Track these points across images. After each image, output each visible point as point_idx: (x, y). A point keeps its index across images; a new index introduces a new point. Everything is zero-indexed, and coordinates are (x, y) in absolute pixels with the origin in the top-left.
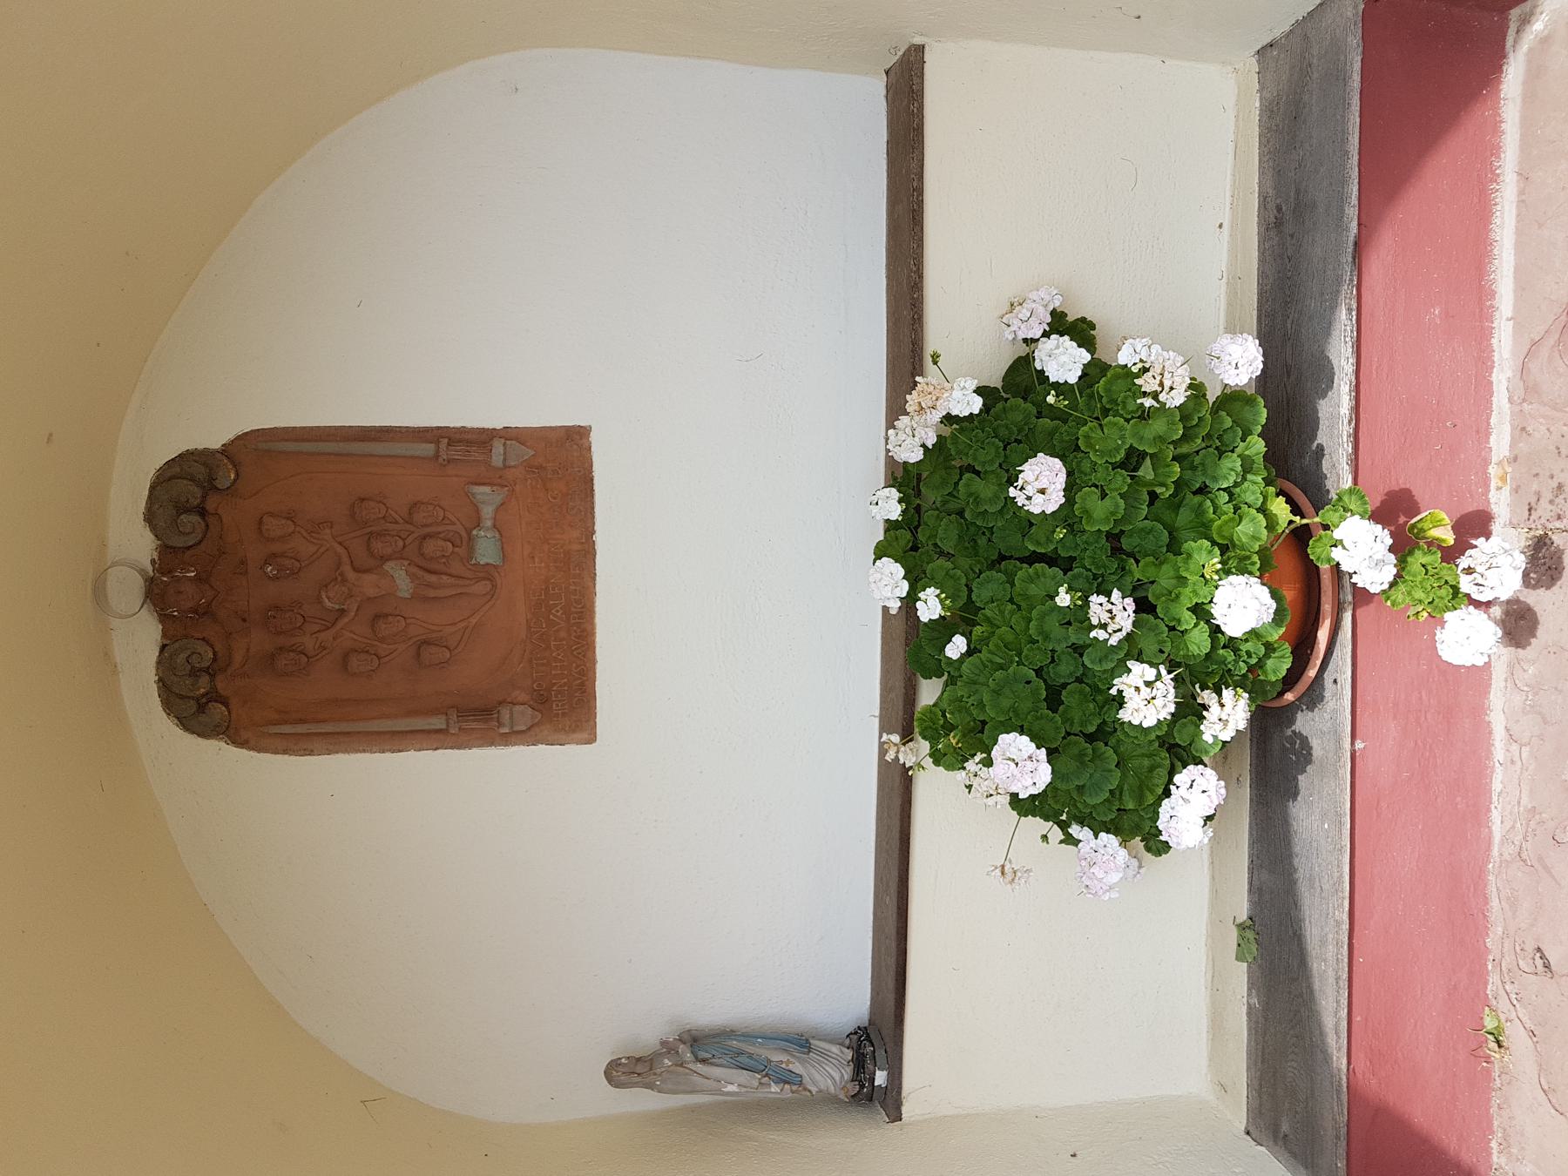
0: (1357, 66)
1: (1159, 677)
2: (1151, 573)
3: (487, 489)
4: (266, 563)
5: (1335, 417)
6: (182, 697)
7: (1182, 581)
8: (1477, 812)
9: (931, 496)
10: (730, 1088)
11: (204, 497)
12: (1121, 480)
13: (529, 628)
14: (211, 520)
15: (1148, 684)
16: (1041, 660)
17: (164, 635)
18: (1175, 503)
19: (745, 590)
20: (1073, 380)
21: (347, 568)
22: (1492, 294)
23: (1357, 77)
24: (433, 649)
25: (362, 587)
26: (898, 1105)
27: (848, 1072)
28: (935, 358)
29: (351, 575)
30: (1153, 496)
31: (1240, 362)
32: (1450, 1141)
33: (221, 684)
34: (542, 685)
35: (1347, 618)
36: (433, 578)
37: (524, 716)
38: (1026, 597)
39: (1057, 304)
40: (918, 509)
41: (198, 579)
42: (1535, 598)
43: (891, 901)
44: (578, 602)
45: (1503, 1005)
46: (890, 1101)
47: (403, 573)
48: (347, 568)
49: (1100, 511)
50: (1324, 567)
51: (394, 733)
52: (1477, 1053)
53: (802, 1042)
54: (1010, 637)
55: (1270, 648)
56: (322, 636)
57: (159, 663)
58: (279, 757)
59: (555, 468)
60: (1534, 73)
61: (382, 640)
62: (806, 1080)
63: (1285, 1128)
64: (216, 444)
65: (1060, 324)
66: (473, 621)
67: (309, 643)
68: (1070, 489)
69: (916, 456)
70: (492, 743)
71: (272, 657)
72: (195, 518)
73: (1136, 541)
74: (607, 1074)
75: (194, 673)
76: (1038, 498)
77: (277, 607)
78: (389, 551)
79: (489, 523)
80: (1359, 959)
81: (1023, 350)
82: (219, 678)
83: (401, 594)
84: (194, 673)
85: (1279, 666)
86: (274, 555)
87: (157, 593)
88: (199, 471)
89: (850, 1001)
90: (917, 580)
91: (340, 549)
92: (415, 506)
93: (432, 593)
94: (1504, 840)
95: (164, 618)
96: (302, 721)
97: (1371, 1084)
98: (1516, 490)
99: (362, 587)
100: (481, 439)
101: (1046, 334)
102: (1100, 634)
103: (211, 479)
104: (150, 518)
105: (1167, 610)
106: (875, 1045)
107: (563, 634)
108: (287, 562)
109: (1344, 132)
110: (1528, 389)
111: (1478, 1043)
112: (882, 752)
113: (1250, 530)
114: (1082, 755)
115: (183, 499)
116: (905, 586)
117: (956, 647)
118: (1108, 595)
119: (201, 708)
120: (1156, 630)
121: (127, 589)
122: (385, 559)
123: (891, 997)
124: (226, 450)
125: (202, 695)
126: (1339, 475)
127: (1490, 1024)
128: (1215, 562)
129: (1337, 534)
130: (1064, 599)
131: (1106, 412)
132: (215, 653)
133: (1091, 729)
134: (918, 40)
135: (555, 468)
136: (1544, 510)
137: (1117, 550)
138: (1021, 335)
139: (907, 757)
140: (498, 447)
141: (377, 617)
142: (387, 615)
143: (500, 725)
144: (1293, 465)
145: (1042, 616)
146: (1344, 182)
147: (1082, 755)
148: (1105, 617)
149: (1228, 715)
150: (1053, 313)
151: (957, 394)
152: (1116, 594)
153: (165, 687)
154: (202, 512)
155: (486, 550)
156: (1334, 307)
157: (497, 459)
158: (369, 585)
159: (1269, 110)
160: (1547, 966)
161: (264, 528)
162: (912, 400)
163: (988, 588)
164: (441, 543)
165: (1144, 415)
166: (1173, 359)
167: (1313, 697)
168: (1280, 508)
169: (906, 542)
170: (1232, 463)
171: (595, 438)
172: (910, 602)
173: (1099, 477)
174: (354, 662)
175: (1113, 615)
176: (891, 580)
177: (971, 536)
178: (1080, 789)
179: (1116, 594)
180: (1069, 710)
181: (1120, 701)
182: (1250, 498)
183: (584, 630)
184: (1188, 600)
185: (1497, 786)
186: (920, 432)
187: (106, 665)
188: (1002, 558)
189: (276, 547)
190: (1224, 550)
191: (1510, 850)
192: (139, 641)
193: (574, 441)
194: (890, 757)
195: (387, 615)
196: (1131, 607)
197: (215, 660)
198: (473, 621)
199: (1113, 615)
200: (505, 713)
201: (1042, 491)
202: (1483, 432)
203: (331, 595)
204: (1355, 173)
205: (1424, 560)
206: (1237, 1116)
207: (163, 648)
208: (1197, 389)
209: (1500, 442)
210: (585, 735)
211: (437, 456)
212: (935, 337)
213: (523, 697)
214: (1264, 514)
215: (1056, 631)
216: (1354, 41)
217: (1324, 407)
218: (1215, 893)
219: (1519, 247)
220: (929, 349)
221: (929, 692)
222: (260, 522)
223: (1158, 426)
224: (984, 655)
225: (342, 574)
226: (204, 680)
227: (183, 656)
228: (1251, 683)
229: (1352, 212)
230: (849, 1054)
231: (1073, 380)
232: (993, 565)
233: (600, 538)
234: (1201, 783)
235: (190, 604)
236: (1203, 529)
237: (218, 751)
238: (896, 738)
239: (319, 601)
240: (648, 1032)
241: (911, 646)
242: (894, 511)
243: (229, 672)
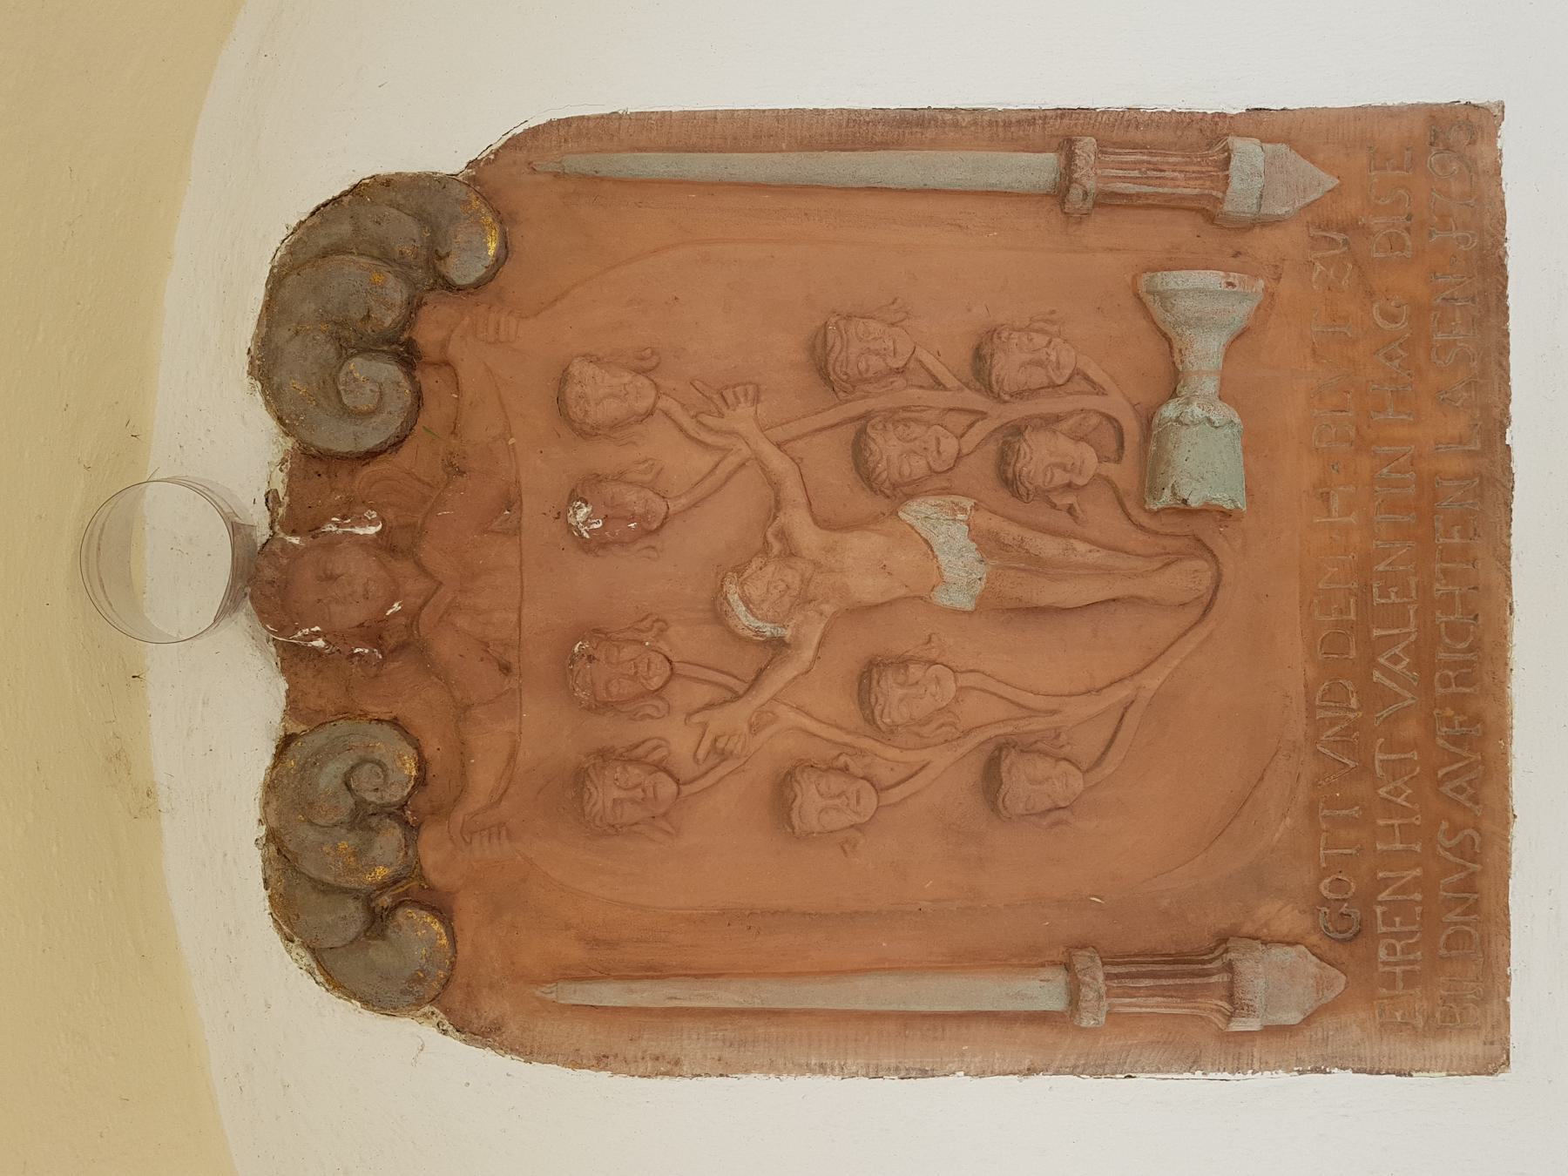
3: (1212, 279)
4: (575, 497)
6: (326, 889)
11: (414, 306)
13: (1311, 709)
14: (430, 380)
17: (294, 707)
21: (798, 521)
24: (1042, 767)
29: (808, 537)
33: (434, 853)
36: (1049, 547)
37: (1279, 979)
41: (386, 546)
44: (1455, 631)
47: (960, 533)
48: (798, 521)
51: (908, 1019)
56: (719, 720)
57: (271, 787)
58: (586, 1074)
61: (887, 735)
64: (450, 159)
66: (1152, 682)
67: (680, 741)
70: (1193, 1063)
71: (580, 778)
72: (388, 371)
75: (363, 818)
77: (598, 633)
78: (918, 466)
79: (1210, 386)
83: (942, 598)
84: (363, 818)
86: (598, 479)
88: (405, 234)
91: (778, 462)
95: (293, 658)
96: (654, 972)
103: (435, 257)
104: (266, 365)
107: (1411, 729)
108: (632, 498)
115: (356, 314)
119: (377, 922)
121: (186, 563)
122: (902, 491)
124: (482, 178)
125: (377, 893)
132: (422, 765)
142: (903, 662)
153: (281, 853)
154: (408, 356)
157: (1241, 195)
158: (862, 564)
161: (573, 391)
164: (1065, 445)
171: (1510, 139)
174: (810, 797)
183: (1477, 719)
187: (121, 777)
189: (603, 456)
192: (221, 711)
193: (1456, 141)
195: (903, 662)
197: (421, 781)
198: (1152, 682)
203: (755, 590)
207: (286, 743)
210: (1471, 1046)
211: (1060, 193)
222: (564, 378)
225: (783, 535)
226: (389, 840)
227: (329, 776)
235: (355, 614)
237: (415, 1047)
239: (718, 614)
243: (459, 816)
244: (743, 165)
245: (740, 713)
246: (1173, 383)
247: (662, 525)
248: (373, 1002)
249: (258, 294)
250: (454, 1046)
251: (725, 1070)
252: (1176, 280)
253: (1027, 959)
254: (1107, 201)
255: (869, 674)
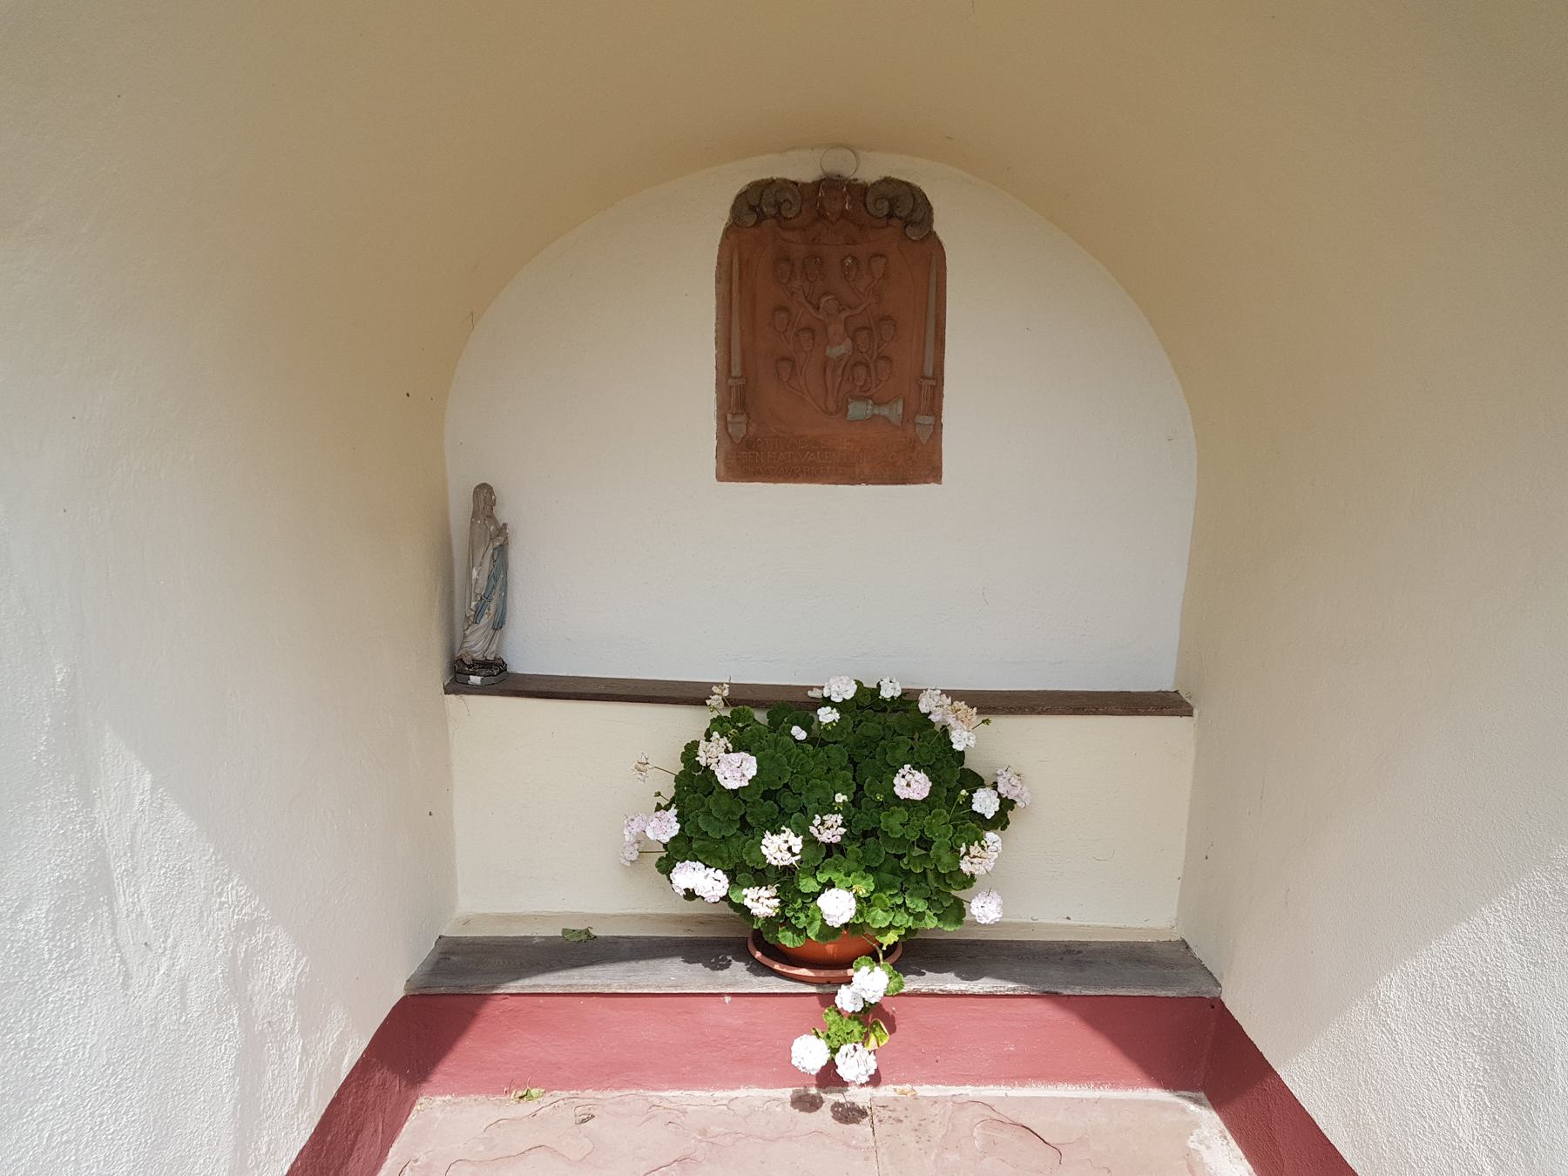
0: (1170, 994)
1: (794, 855)
2: (852, 856)
4: (854, 258)
5: (946, 982)
7: (848, 875)
8: (680, 1080)
9: (892, 719)
10: (475, 573)
12: (913, 836)
15: (790, 849)
16: (794, 786)
17: (805, 184)
18: (894, 872)
19: (826, 589)
20: (975, 807)
22: (1022, 1085)
23: (1162, 993)
25: (830, 323)
26: (456, 692)
27: (478, 656)
28: (986, 722)
29: (843, 315)
30: (900, 857)
31: (984, 910)
32: (447, 1066)
33: (770, 222)
34: (758, 445)
35: (813, 989)
36: (839, 371)
37: (739, 430)
38: (833, 778)
39: (1020, 804)
40: (884, 710)
41: (844, 210)
42: (826, 1109)
43: (601, 689)
45: (548, 1099)
46: (459, 686)
49: (893, 823)
50: (850, 972)
51: (729, 340)
52: (512, 1084)
53: (499, 625)
54: (808, 768)
55: (801, 932)
57: (785, 181)
59: (912, 458)
60: (1163, 1106)
62: (475, 627)
63: (454, 958)
64: (936, 227)
65: (1007, 804)
67: (796, 284)
68: (909, 803)
69: (923, 708)
71: (787, 259)
73: (872, 847)
74: (484, 485)
75: (778, 205)
76: (904, 782)
80: (582, 1001)
81: (988, 781)
82: (774, 222)
84: (778, 205)
85: (788, 940)
87: (831, 184)
88: (918, 216)
89: (524, 660)
90: (841, 707)
92: (888, 359)
93: (829, 372)
94: (661, 1098)
95: (817, 185)
97: (491, 1010)
98: (895, 1099)
99: (830, 323)
100: (935, 409)
101: (999, 796)
102: (817, 822)
103: (913, 223)
104: (887, 181)
105: (829, 865)
106: (478, 673)
109: (1129, 986)
110: (961, 1104)
111: (517, 1083)
112: (717, 684)
113: (879, 918)
114: (733, 813)
116: (839, 700)
117: (799, 733)
118: (843, 825)
119: (752, 208)
120: (821, 856)
122: (853, 339)
123: (532, 688)
124: (932, 234)
126: (912, 984)
127: (534, 1092)
128: (863, 893)
129: (877, 969)
130: (840, 798)
131: (955, 827)
133: (749, 819)
134: (1196, 712)
135: (912, 458)
136: (885, 1114)
137: (865, 834)
138: (1000, 780)
139: (715, 701)
140: (929, 420)
141: (813, 331)
143: (734, 415)
144: (912, 954)
145: (823, 787)
146: (1096, 986)
147: (733, 813)
148: (829, 824)
149: (762, 902)
150: (1013, 802)
151: (965, 734)
152: (843, 830)
154: (890, 216)
155: (857, 410)
156: (1016, 981)
157: (920, 419)
159: (1145, 947)
160: (584, 1121)
162: (962, 705)
163: (837, 754)
165: (954, 850)
166: (990, 866)
167: (760, 969)
168: (891, 938)
169: (867, 702)
170: (921, 906)
171: (933, 486)
172: (827, 701)
173: (915, 821)
174: (783, 315)
175: (830, 830)
176: (843, 690)
177: (870, 744)
178: (709, 813)
179: (843, 830)
180: (772, 802)
181: (776, 832)
182: (898, 918)
184: (835, 876)
185: (697, 1093)
186: (940, 710)
188: (855, 764)
190: (867, 900)
191: (657, 1102)
192: (803, 169)
194: (715, 689)
196: (834, 840)
199: (830, 830)
200: (742, 418)
201: (908, 785)
202: (933, 1080)
204: (1101, 993)
205: (856, 1033)
206: (449, 931)
207: (796, 183)
208: (969, 881)
209: (925, 1090)
212: (1000, 723)
213: (752, 430)
214: (889, 925)
215: (819, 794)
216: (1186, 991)
217: (951, 976)
218: (604, 917)
219: (1054, 1099)
220: (992, 718)
221: (761, 716)
223: (947, 858)
224: (796, 751)
226: (773, 211)
227: (789, 197)
228: (781, 921)
229: (1077, 991)
230: (491, 658)
231: (975, 807)
232: (851, 760)
233: (863, 487)
234: (718, 886)
236: (880, 888)
238: (726, 693)
239: (825, 294)
240: (504, 514)
241: (794, 705)
242: (886, 693)
244: (933, 290)
245: (802, 299)
246: (877, 404)
247: (841, 146)
248: (734, 207)
249: (904, 179)
250: (723, 227)
251: (718, 294)
252: (900, 404)
253: (744, 369)
254: (920, 387)
255: (809, 329)
